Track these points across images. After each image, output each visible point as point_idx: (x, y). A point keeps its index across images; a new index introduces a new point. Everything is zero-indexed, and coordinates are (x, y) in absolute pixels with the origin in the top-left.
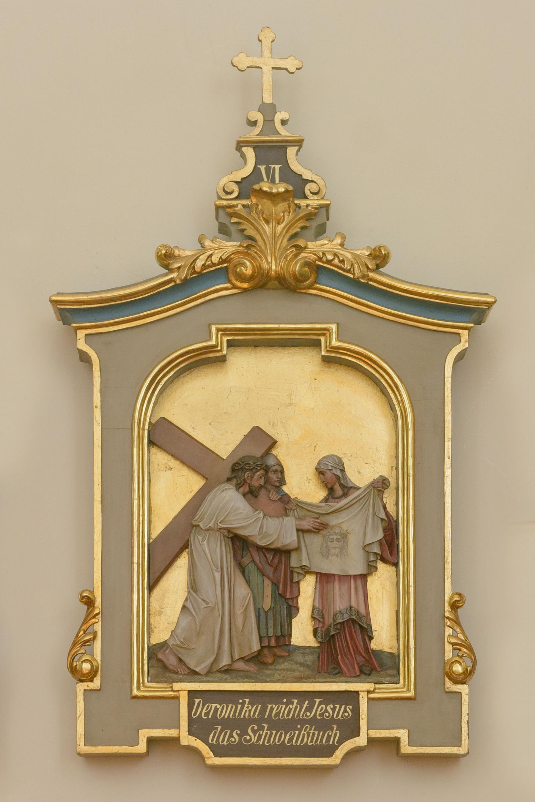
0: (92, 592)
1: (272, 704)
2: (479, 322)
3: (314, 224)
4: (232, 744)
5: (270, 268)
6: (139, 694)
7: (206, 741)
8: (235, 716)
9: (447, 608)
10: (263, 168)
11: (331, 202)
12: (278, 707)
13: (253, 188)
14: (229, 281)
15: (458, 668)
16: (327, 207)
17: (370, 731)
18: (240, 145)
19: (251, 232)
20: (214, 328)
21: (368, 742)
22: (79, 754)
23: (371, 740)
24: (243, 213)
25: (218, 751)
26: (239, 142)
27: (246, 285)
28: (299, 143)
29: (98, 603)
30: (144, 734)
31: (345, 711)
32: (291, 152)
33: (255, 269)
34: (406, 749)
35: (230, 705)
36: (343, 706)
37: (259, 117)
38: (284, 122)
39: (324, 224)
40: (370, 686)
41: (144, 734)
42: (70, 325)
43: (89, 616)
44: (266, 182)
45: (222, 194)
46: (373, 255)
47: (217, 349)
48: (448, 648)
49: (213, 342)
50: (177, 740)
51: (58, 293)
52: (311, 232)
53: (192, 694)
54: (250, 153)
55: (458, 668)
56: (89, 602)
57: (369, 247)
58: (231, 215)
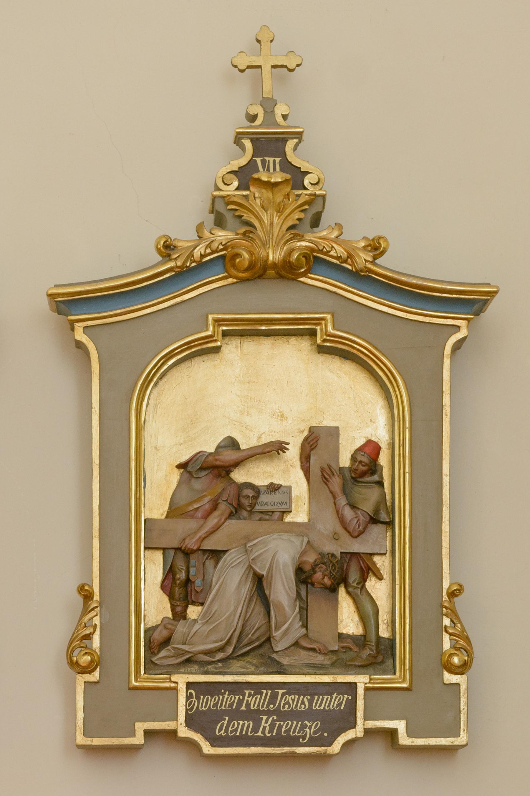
0: (91, 587)
2: (477, 314)
5: (268, 257)
8: (226, 707)
9: (445, 597)
10: (258, 160)
11: (326, 191)
13: (252, 177)
14: (226, 271)
15: (456, 660)
16: (324, 197)
17: (366, 722)
18: (238, 139)
19: (247, 216)
20: (210, 317)
21: (365, 732)
23: (367, 731)
25: (215, 741)
26: (239, 133)
27: (244, 275)
28: (299, 136)
29: (96, 598)
30: (140, 727)
32: (290, 144)
34: (404, 740)
37: (258, 110)
38: (285, 117)
41: (140, 727)
43: (86, 611)
46: (373, 245)
47: (214, 338)
48: (446, 638)
49: (210, 333)
50: (174, 732)
51: (55, 286)
53: (189, 685)
54: (248, 143)
55: (456, 660)
56: (88, 597)
58: (228, 204)
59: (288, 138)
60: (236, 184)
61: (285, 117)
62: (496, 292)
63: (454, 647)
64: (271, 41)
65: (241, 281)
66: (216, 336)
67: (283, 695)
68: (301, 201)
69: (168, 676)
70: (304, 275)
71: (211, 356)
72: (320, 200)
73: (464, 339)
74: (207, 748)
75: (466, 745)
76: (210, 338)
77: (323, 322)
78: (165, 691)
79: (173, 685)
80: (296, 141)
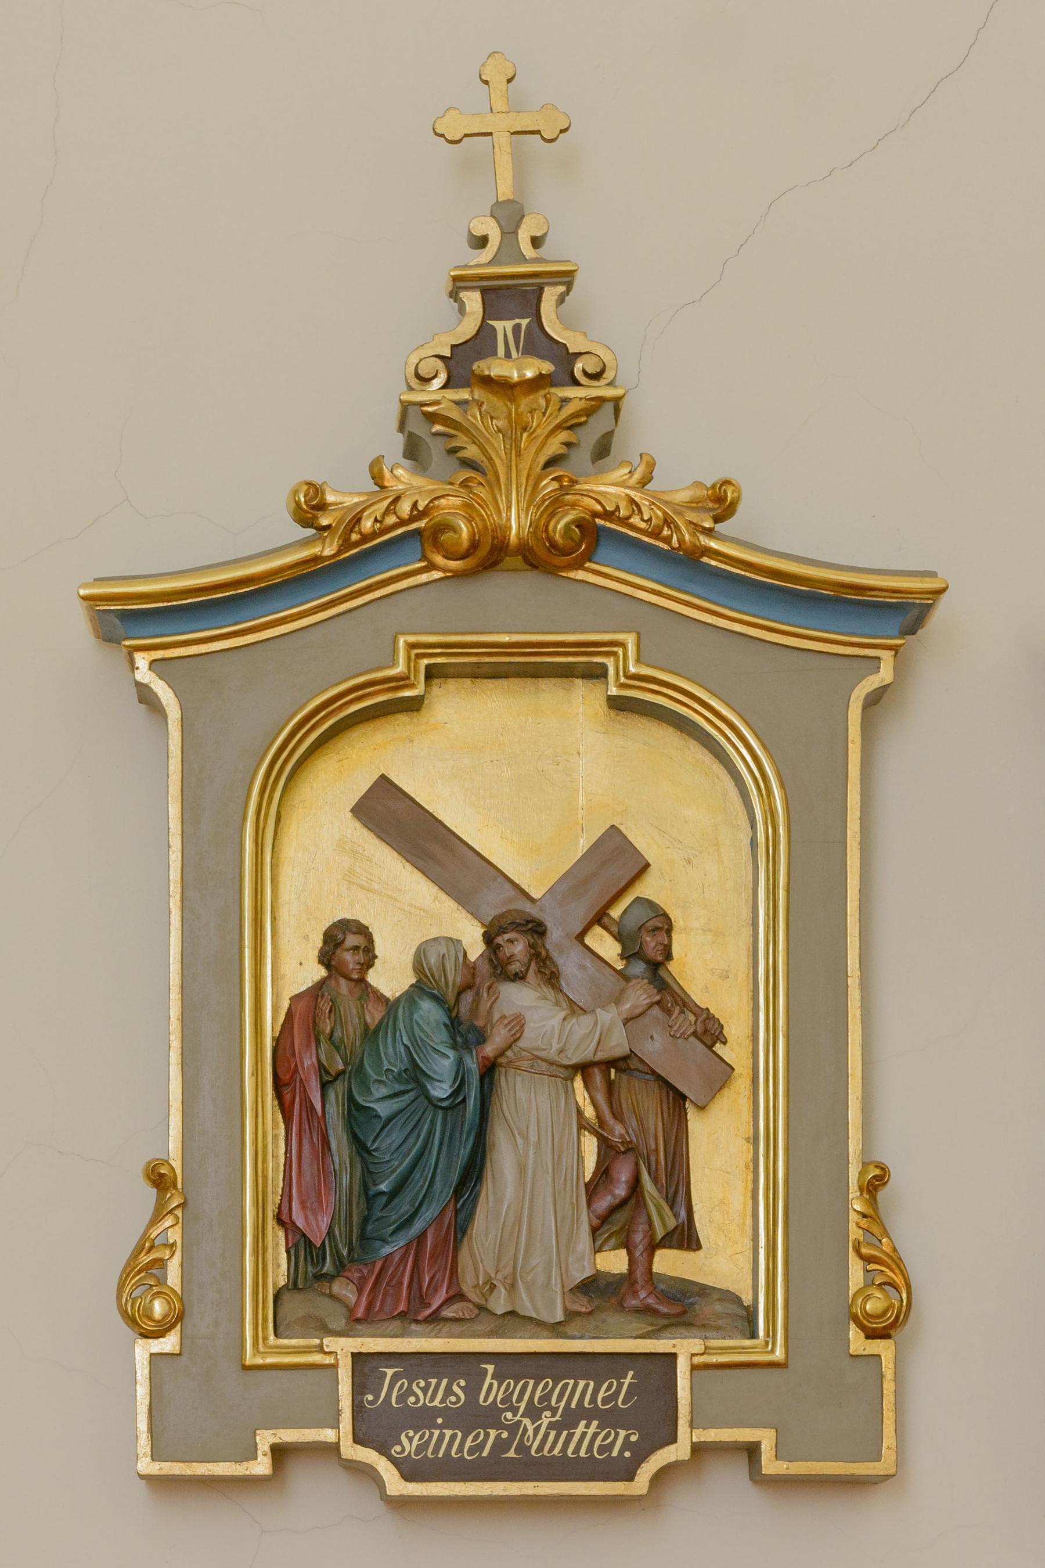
1: (587, 1380)
2: (911, 630)
3: (589, 436)
4: (398, 1456)
6: (259, 1361)
7: (383, 1450)
12: (507, 1385)
16: (617, 403)
18: (459, 284)
19: (471, 452)
20: (401, 641)
22: (142, 1477)
23: (697, 1449)
24: (455, 414)
25: (410, 1471)
28: (566, 278)
31: (449, 1391)
32: (550, 295)
33: (474, 530)
34: (770, 1465)
35: (582, 1383)
36: (445, 1382)
38: (536, 242)
39: (609, 436)
40: (696, 1345)
42: (119, 644)
44: (500, 358)
45: (414, 383)
49: (400, 669)
50: (334, 1448)
52: (583, 456)
54: (473, 301)
57: (698, 484)
59: (544, 283)
60: (442, 378)
61: (536, 242)
62: (942, 591)
63: (869, 1284)
64: (509, 81)
65: (458, 575)
66: (413, 657)
67: (395, 1378)
68: (569, 410)
69: (317, 1341)
70: (579, 565)
71: (403, 718)
72: (609, 407)
73: (883, 690)
74: (395, 1484)
75: (894, 1475)
76: (402, 681)
77: (620, 651)
78: (273, 1372)
79: (329, 1360)
80: (562, 289)
